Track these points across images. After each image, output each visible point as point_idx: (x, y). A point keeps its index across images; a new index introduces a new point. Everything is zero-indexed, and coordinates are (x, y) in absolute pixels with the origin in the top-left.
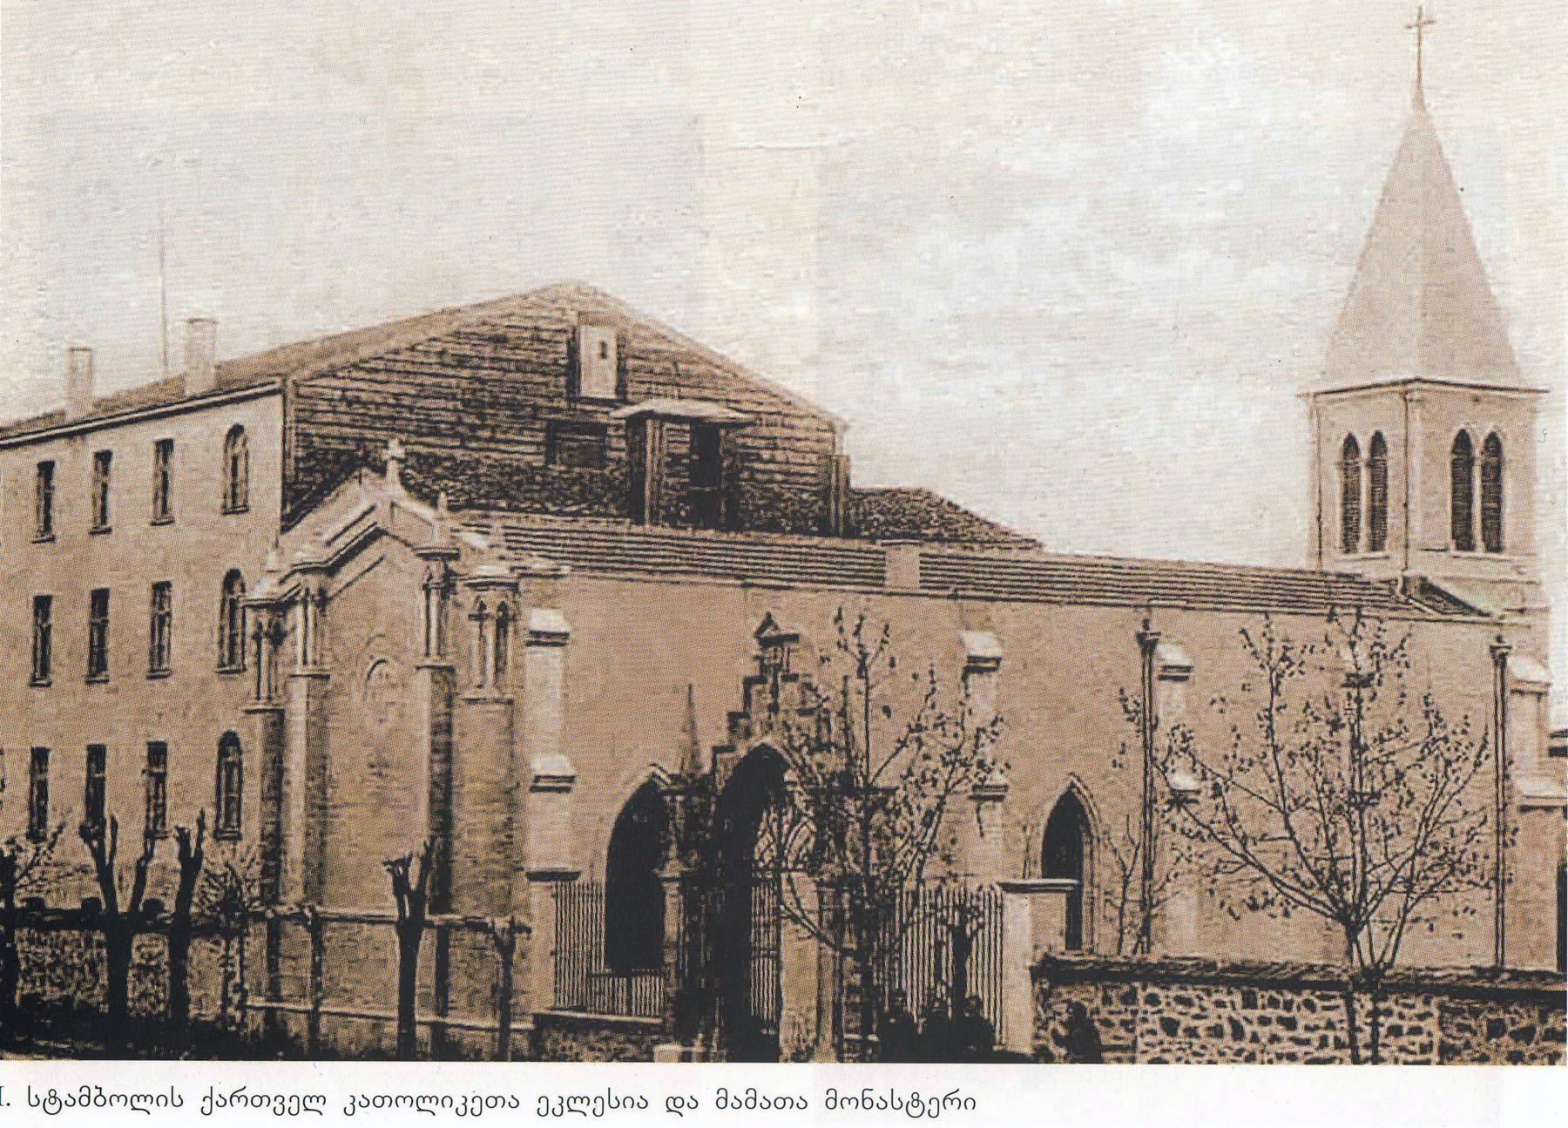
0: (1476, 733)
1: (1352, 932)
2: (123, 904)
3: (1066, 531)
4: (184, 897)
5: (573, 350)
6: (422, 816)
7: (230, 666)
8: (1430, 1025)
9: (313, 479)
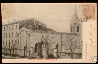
0: (78, 41)
1: (71, 51)
2: (11, 48)
3: (58, 31)
4: (14, 48)
5: (33, 21)
6: (25, 44)
7: (16, 37)
8: (75, 56)
9: (20, 27)
